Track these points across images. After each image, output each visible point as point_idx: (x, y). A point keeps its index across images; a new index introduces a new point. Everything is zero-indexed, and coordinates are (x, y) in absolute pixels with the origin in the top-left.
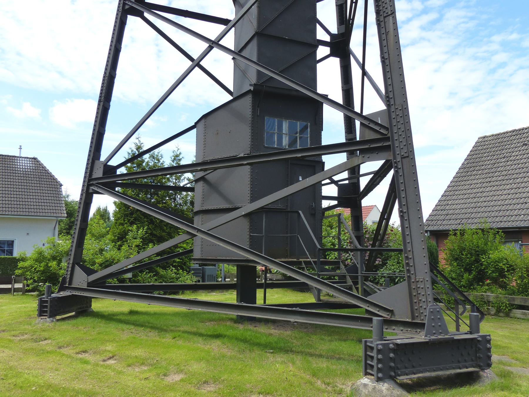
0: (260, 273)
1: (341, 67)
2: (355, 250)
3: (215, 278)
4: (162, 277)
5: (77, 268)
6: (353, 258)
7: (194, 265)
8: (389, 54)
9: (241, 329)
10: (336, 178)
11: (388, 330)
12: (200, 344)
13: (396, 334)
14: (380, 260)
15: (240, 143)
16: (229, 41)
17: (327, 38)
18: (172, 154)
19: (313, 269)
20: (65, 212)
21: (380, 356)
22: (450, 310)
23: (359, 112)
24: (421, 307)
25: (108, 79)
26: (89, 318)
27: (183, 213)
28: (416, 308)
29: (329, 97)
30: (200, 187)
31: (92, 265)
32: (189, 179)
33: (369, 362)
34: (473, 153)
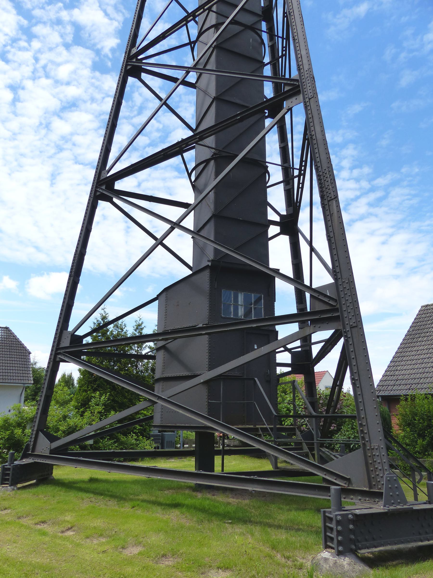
0: (218, 438)
1: (290, 244)
2: (310, 416)
3: (173, 444)
4: (122, 443)
5: (41, 435)
6: (308, 424)
7: (155, 432)
8: (334, 233)
9: (200, 498)
10: (289, 346)
11: (346, 500)
12: (158, 513)
13: (354, 504)
14: (335, 425)
15: (198, 312)
16: (189, 222)
17: (277, 219)
18: (135, 324)
19: (270, 435)
20: (32, 379)
21: (339, 528)
22: (406, 477)
23: (309, 285)
24: (378, 475)
25: (79, 256)
26: (49, 486)
27: (144, 380)
28: (373, 476)
29: (280, 271)
30: (160, 355)
31: (56, 432)
32: (150, 347)
33: (328, 534)
34: (417, 321)
